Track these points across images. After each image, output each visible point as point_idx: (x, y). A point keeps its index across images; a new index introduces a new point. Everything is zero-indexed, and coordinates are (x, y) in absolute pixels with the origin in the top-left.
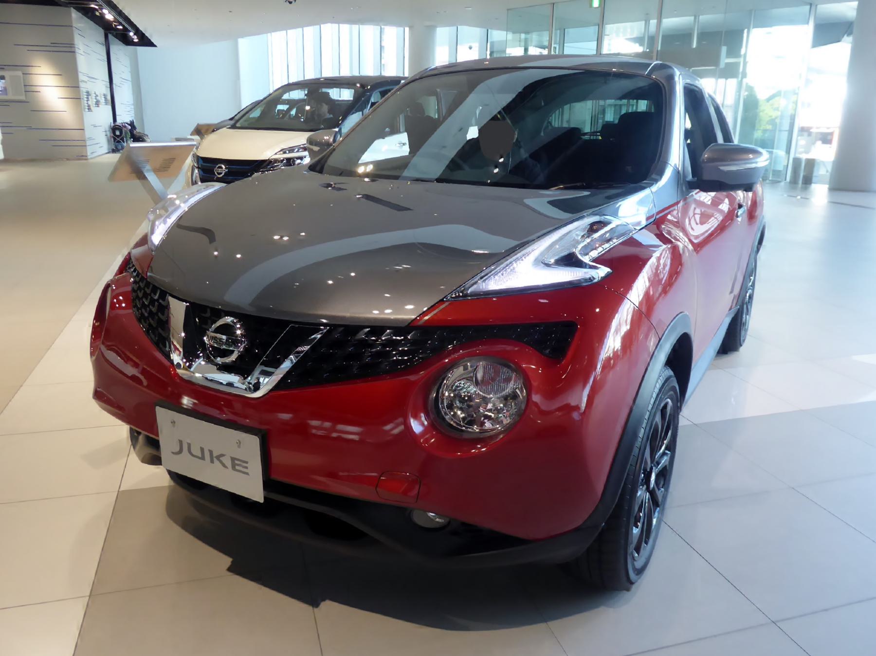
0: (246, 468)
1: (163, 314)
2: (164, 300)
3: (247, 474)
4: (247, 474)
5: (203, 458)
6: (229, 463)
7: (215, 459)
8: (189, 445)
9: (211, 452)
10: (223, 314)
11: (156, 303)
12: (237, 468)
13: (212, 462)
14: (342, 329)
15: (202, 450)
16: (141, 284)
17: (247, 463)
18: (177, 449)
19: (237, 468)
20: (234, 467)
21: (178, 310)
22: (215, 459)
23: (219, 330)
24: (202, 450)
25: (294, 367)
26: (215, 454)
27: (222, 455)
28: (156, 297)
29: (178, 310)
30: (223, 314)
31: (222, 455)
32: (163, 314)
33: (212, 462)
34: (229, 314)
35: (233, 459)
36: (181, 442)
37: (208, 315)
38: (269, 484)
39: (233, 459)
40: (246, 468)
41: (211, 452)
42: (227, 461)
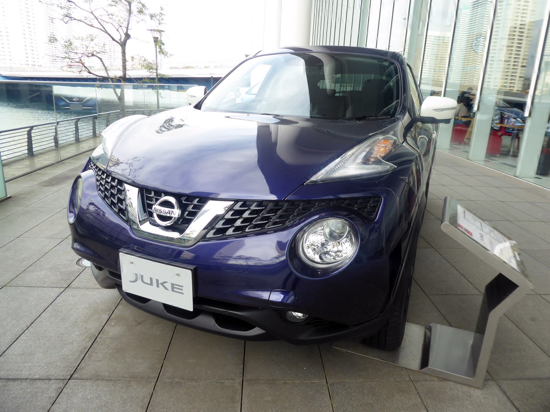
0: (182, 290)
1: (122, 204)
2: (121, 186)
3: (182, 293)
4: (182, 293)
5: (151, 284)
7: (160, 285)
8: (142, 276)
9: (157, 281)
10: (163, 194)
11: (116, 197)
12: (175, 290)
13: (158, 286)
14: (256, 203)
15: (151, 279)
16: (102, 176)
17: (182, 286)
18: (133, 279)
19: (175, 290)
20: (173, 290)
21: (132, 195)
22: (160, 285)
23: (170, 218)
24: (151, 279)
25: (295, 311)
26: (160, 282)
27: (165, 282)
28: (115, 193)
29: (132, 195)
30: (163, 194)
31: (165, 282)
32: (122, 204)
33: (158, 286)
34: (167, 194)
35: (173, 285)
36: (136, 275)
37: (152, 195)
38: (196, 300)
39: (173, 285)
40: (182, 290)
41: (157, 281)
42: (168, 286)
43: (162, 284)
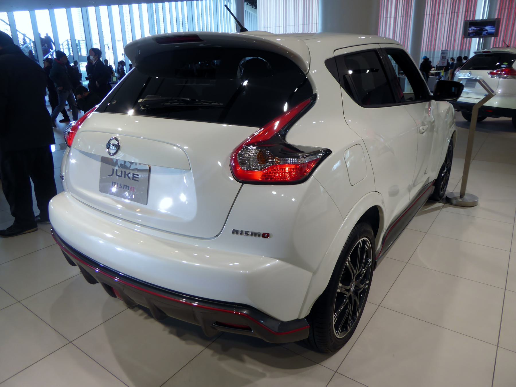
3: (138, 181)
4: (138, 181)
5: (121, 176)
6: (131, 178)
9: (125, 172)
12: (135, 178)
13: (125, 177)
19: (135, 178)
27: (130, 173)
33: (125, 177)
35: (134, 174)
39: (134, 174)
43: (127, 175)
